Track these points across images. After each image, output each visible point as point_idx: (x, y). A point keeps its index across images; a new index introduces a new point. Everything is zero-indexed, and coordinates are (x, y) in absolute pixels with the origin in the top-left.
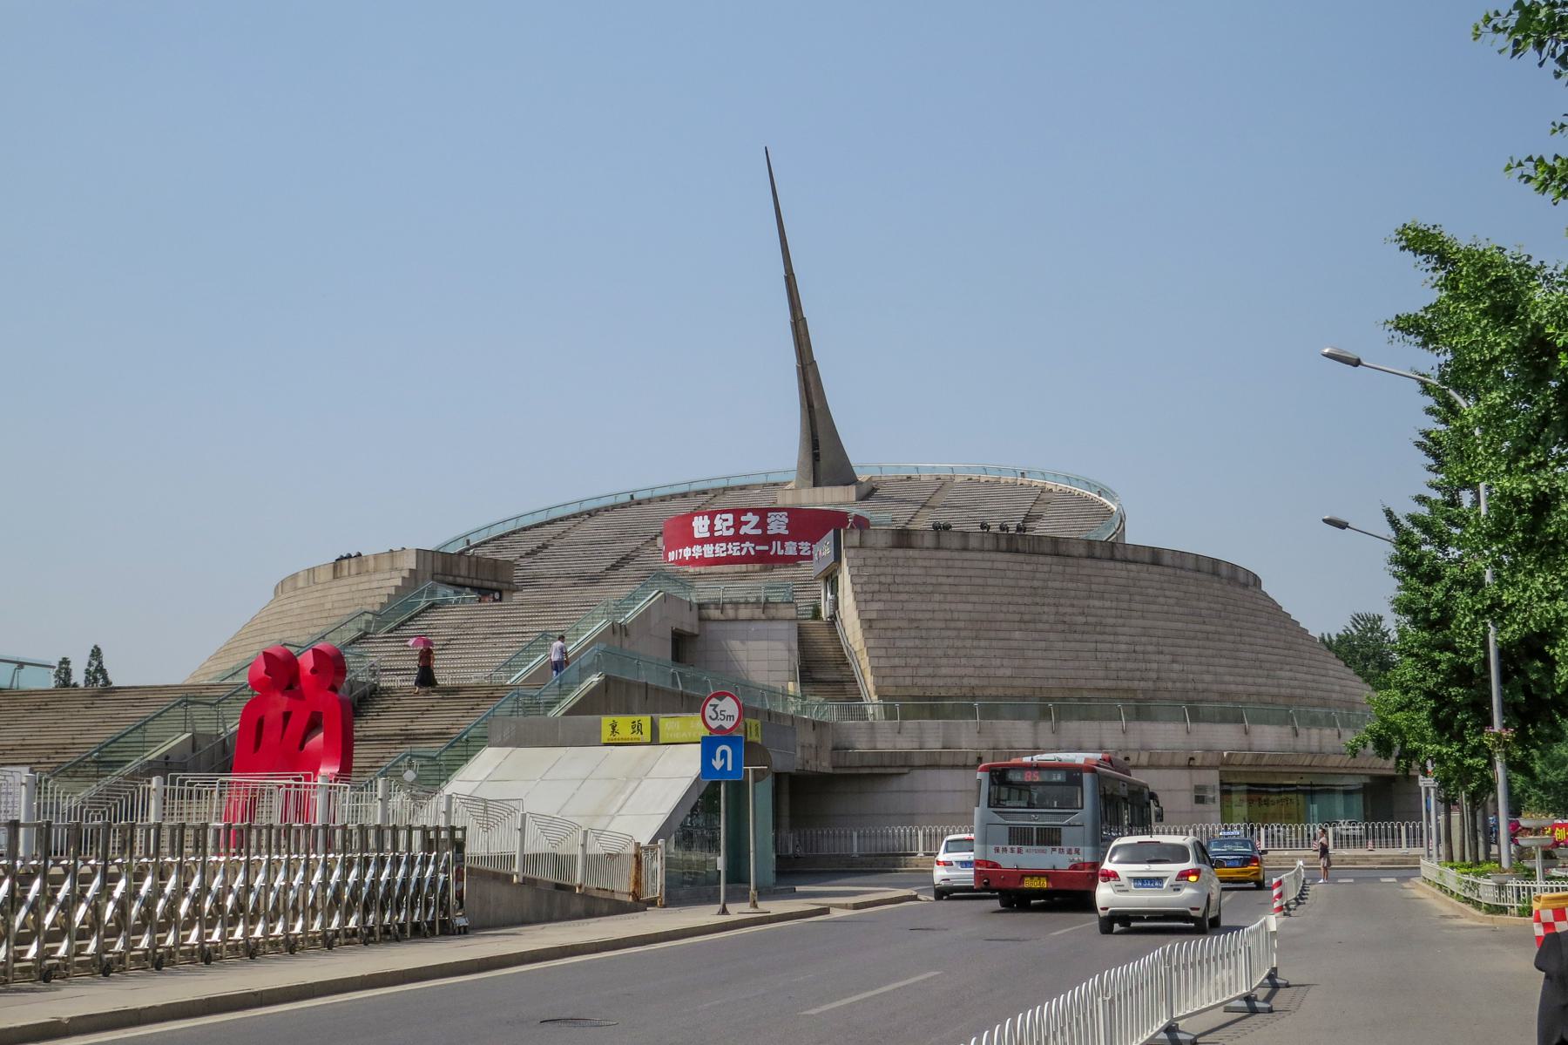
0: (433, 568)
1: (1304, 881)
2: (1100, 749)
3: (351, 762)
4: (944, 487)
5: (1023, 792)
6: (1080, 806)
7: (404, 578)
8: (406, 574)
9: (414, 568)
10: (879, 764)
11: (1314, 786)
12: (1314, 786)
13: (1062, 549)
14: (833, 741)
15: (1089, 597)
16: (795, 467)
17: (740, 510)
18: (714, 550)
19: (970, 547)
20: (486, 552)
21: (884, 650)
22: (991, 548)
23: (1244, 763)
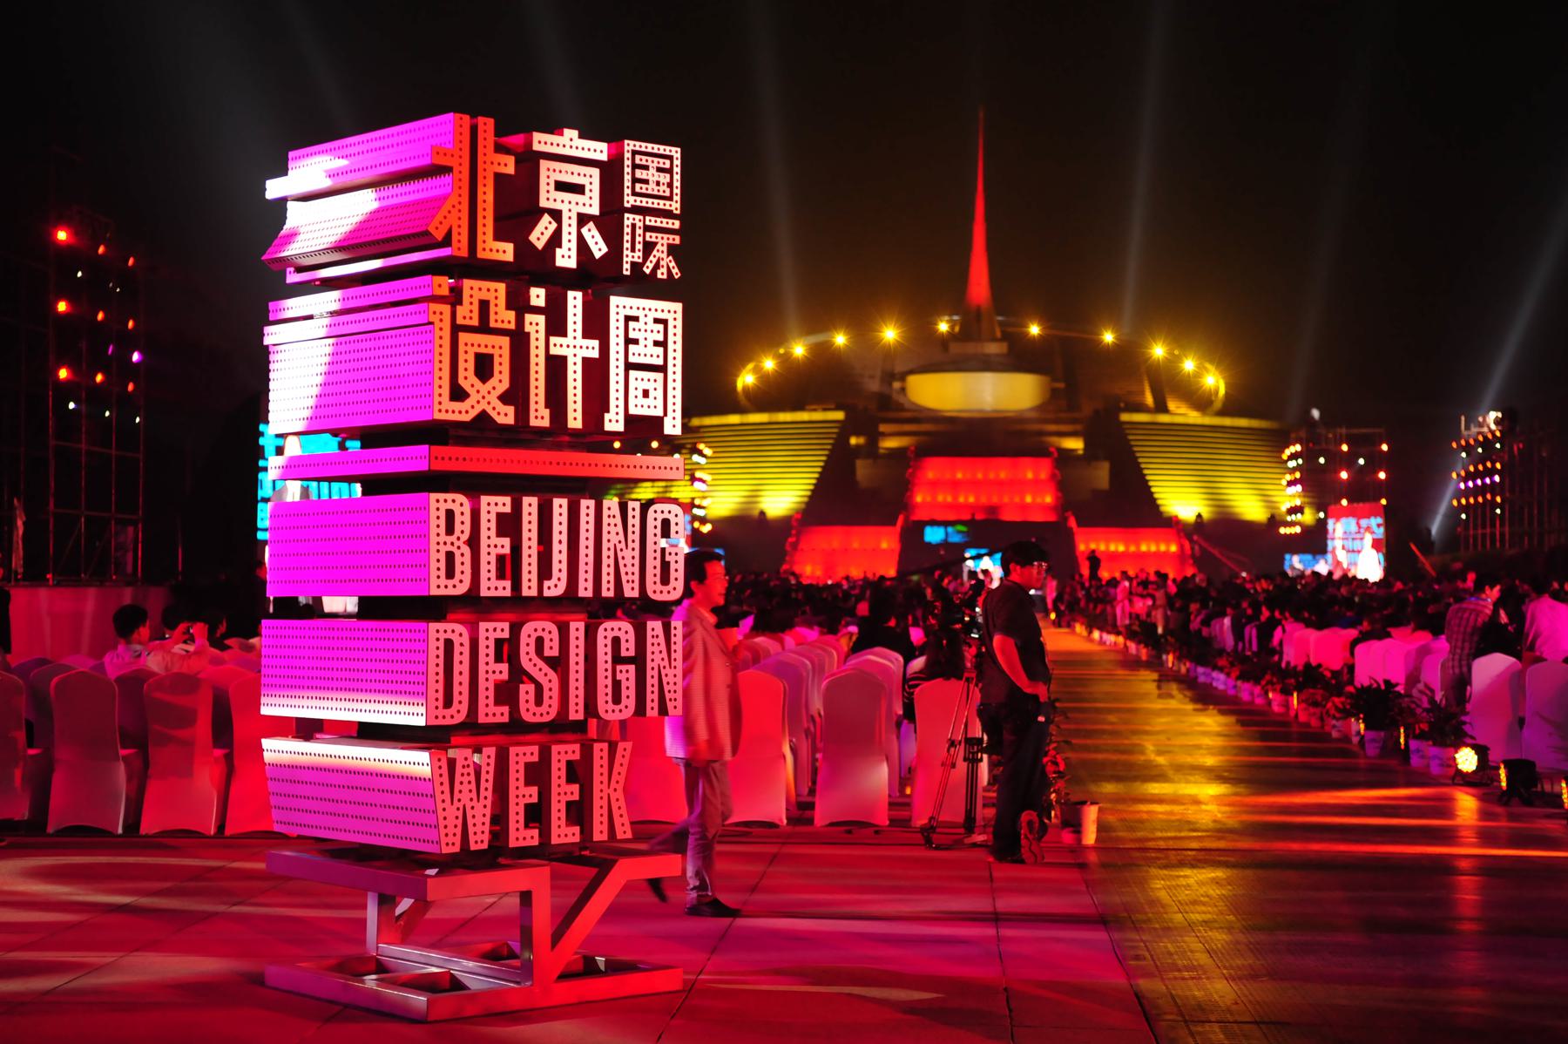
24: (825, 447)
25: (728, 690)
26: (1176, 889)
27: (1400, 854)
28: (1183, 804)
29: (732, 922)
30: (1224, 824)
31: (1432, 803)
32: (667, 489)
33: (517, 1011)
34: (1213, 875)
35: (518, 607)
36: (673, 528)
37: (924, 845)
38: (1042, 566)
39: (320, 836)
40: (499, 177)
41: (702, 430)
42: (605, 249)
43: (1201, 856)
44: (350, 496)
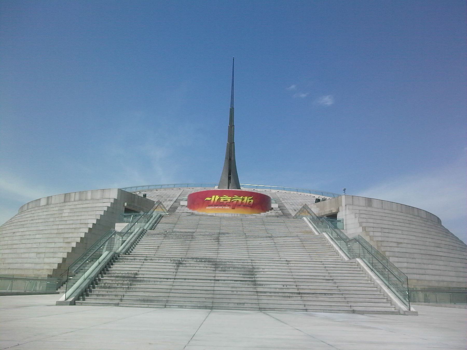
0: (308, 310)
1: (244, 214)
2: (74, 296)
3: (219, 206)
4: (227, 235)
5: (234, 216)
6: (363, 228)
7: (77, 243)
8: (112, 201)
9: (99, 219)
10: (386, 214)
11: (182, 266)
12: (182, 266)
13: (353, 312)
14: (449, 302)
15: (219, 235)
16: (272, 204)
17: (130, 210)
18: (149, 188)
19: (221, 268)
20: (124, 190)
21: (465, 289)
22: (72, 194)
23: (159, 206)
24: (157, 228)
25: (452, 303)
26: (156, 226)
27: (21, 292)
28: (126, 240)
29: (274, 203)
30: (264, 313)
31: (312, 223)
32: (148, 306)
33: (200, 308)
34: (337, 249)
35: (388, 274)
36: (157, 191)
37: (436, 302)
38: (325, 217)
39: (454, 308)
40: (218, 188)
41: (169, 302)
42: (213, 196)
43: (236, 306)
44: (273, 203)
